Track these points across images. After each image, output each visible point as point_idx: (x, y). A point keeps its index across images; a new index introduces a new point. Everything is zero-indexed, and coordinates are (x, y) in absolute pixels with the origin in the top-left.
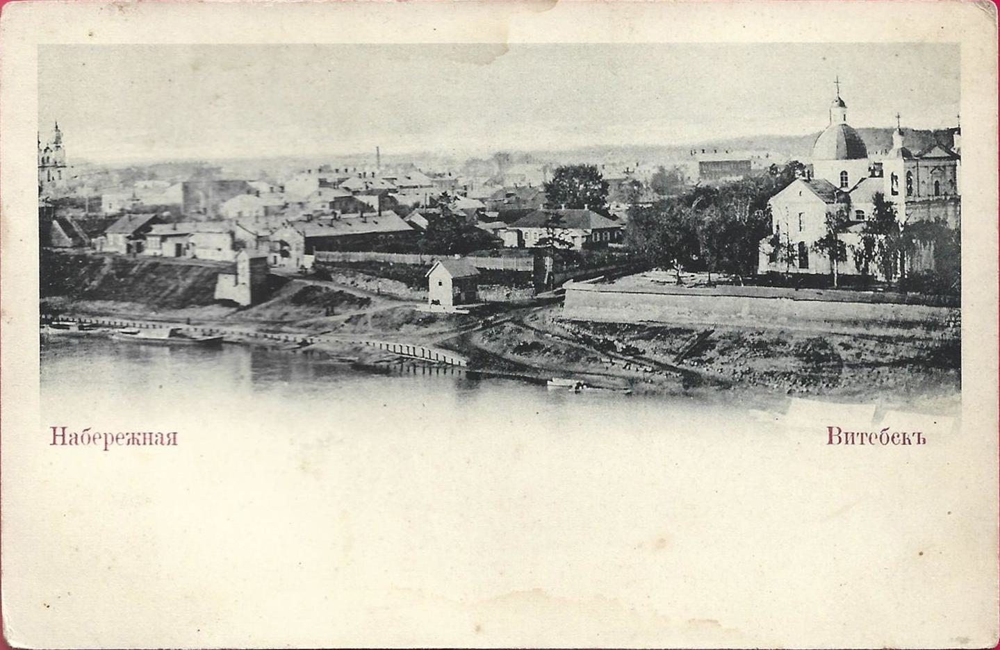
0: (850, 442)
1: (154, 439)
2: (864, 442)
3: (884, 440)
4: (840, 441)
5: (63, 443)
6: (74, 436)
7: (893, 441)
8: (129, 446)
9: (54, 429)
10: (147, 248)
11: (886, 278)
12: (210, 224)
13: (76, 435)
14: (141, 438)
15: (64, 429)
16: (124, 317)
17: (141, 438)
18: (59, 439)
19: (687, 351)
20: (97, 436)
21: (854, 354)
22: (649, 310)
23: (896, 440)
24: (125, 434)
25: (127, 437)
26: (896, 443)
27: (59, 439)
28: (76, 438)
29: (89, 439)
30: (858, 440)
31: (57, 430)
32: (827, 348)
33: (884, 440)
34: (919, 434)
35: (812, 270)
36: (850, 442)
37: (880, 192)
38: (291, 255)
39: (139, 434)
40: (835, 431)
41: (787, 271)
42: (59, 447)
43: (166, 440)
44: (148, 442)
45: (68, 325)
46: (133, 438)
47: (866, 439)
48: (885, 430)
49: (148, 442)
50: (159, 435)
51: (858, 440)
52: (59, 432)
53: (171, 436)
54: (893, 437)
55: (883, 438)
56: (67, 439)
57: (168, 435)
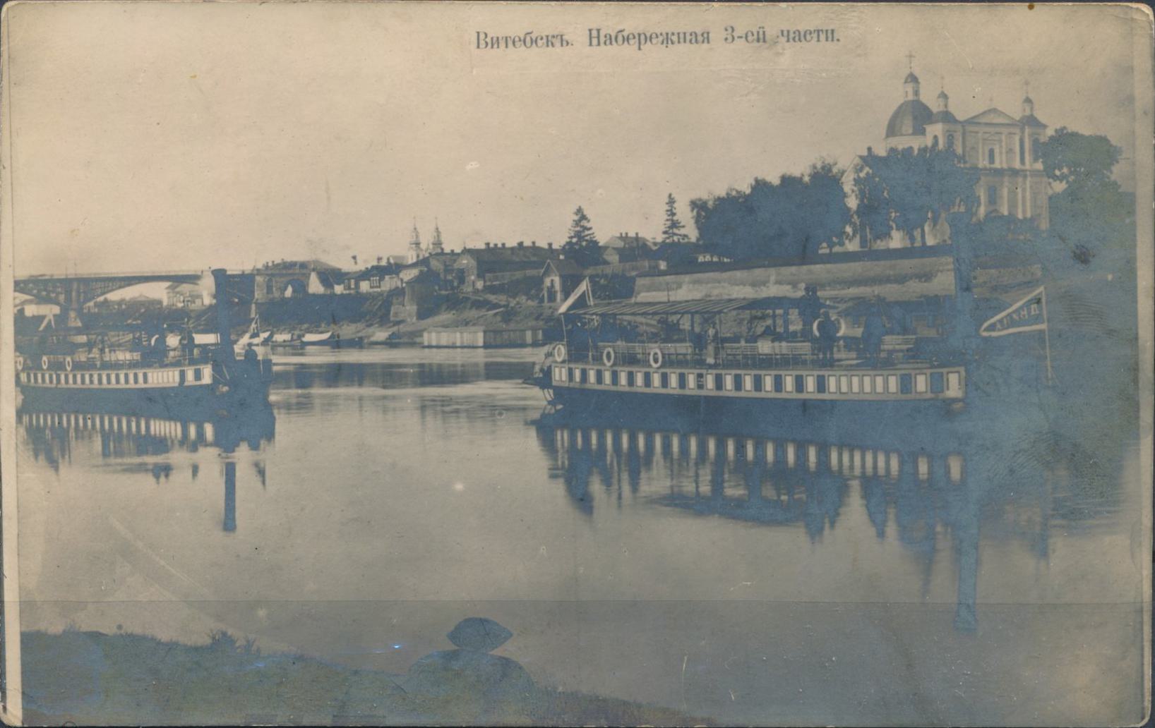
2: (821, 39)
3: (528, 44)
4: (486, 46)
5: (599, 44)
6: (608, 36)
7: (651, 40)
9: (590, 30)
10: (714, 196)
11: (917, 228)
12: (12, 373)
13: (610, 36)
14: (675, 38)
17: (675, 38)
18: (595, 41)
23: (540, 42)
24: (659, 34)
26: (539, 45)
27: (595, 41)
28: (611, 39)
33: (528, 44)
34: (562, 36)
35: (997, 165)
37: (759, 178)
39: (673, 34)
40: (482, 36)
41: (669, 300)
43: (700, 38)
46: (667, 39)
48: (621, 31)
52: (594, 33)
53: (705, 35)
55: (530, 42)
56: (602, 39)
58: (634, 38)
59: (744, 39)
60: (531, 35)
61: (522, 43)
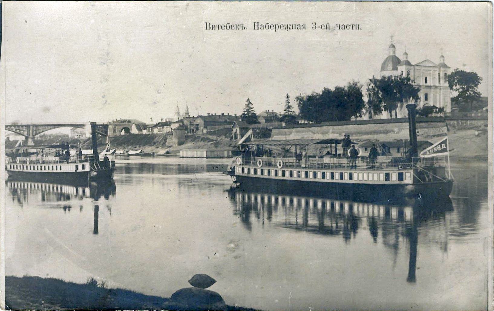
0: (357, 28)
1: (296, 27)
6: (262, 26)
8: (219, 30)
13: (263, 25)
14: (291, 27)
15: (258, 23)
16: (48, 146)
17: (291, 27)
18: (256, 28)
19: (402, 159)
20: (272, 26)
21: (317, 179)
22: (187, 102)
23: (233, 27)
25: (285, 27)
27: (256, 28)
29: (278, 27)
30: (217, 28)
31: (255, 24)
32: (374, 148)
36: (357, 28)
38: (390, 75)
42: (257, 31)
43: (302, 27)
44: (294, 28)
45: (462, 138)
47: (220, 27)
48: (267, 24)
49: (294, 28)
50: (343, 26)
51: (217, 28)
52: (256, 24)
54: (280, 26)
57: (303, 26)
58: (224, 26)
59: (320, 28)
60: (269, 24)
61: (225, 28)
